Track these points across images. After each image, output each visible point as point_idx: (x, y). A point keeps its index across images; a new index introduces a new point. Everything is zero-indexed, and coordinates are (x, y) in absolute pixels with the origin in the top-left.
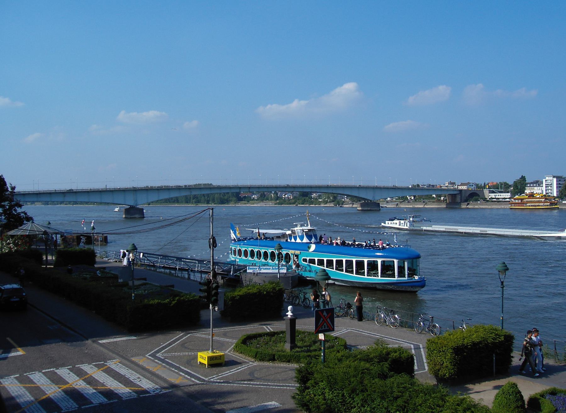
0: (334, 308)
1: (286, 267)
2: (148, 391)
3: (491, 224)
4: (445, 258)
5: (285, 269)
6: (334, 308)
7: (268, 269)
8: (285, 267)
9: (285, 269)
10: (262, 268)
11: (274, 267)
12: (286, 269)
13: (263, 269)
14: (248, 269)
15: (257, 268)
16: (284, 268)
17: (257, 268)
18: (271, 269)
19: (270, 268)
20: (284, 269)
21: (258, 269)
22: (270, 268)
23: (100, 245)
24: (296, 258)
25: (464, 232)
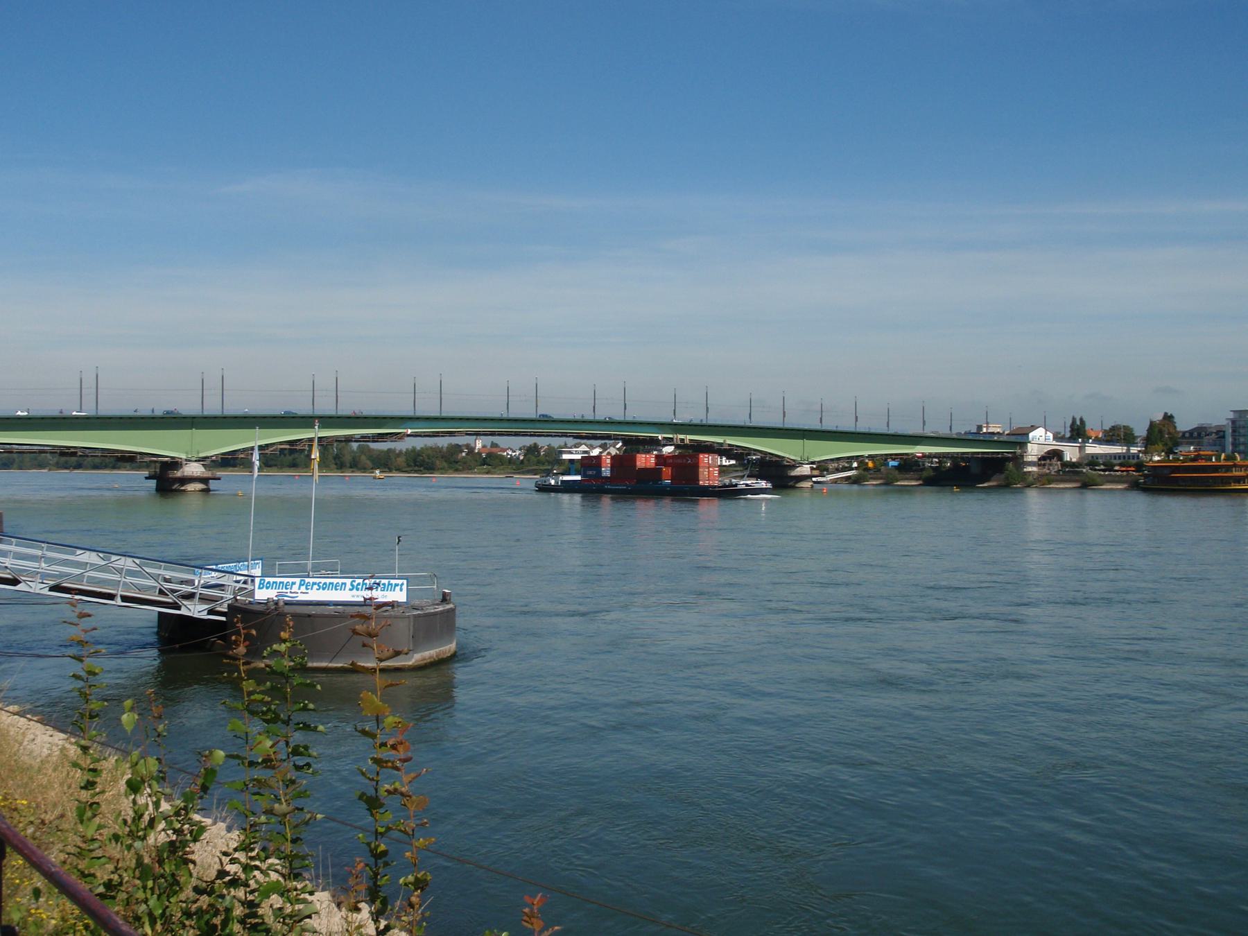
0: (220, 868)
1: (405, 581)
2: (149, 920)
3: (139, 468)
4: (1109, 601)
5: (401, 590)
6: (220, 868)
7: (336, 587)
8: (400, 582)
9: (401, 590)
10: (314, 584)
11: (361, 581)
12: (405, 587)
13: (316, 587)
14: (259, 588)
15: (294, 583)
16: (396, 585)
17: (294, 583)
18: (349, 586)
19: (345, 584)
20: (398, 588)
21: (295, 588)
22: (345, 584)
23: (323, 464)
24: (1058, 460)
25: (1124, 426)
